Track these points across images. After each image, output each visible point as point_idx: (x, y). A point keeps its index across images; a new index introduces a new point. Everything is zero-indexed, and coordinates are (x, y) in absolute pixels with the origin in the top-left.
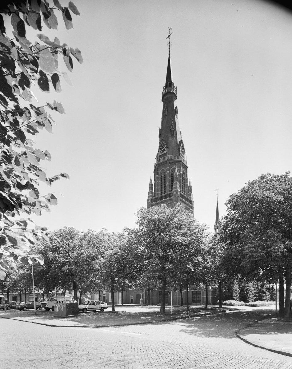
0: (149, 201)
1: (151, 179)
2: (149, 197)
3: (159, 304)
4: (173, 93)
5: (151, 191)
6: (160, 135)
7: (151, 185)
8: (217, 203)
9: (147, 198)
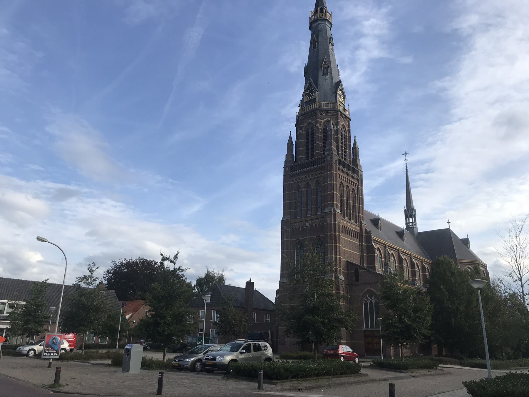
1: (290, 137)
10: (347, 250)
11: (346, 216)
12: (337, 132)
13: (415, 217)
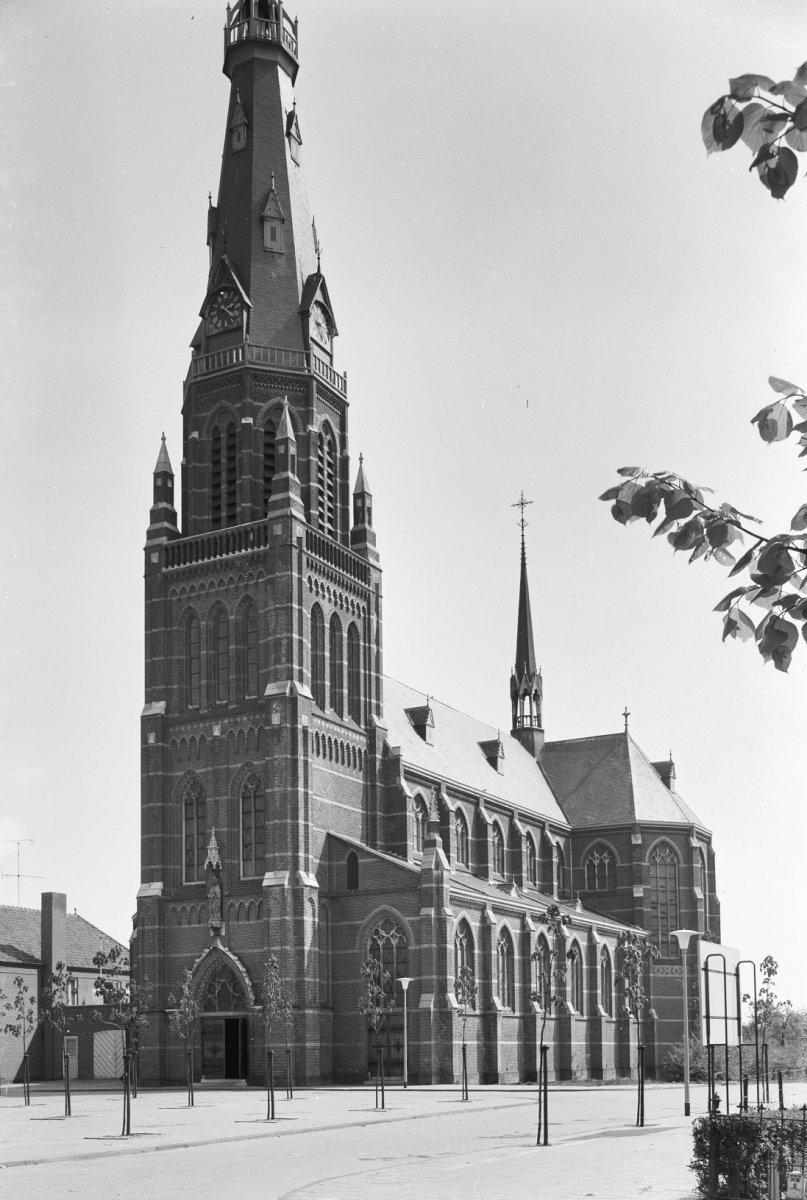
0: (155, 559)
1: (164, 450)
2: (151, 534)
3: (203, 1081)
4: (276, 46)
5: (163, 505)
6: (214, 237)
7: (163, 477)
8: (523, 554)
9: (143, 541)
10: (329, 801)
11: (327, 704)
12: (304, 442)
13: (537, 697)
